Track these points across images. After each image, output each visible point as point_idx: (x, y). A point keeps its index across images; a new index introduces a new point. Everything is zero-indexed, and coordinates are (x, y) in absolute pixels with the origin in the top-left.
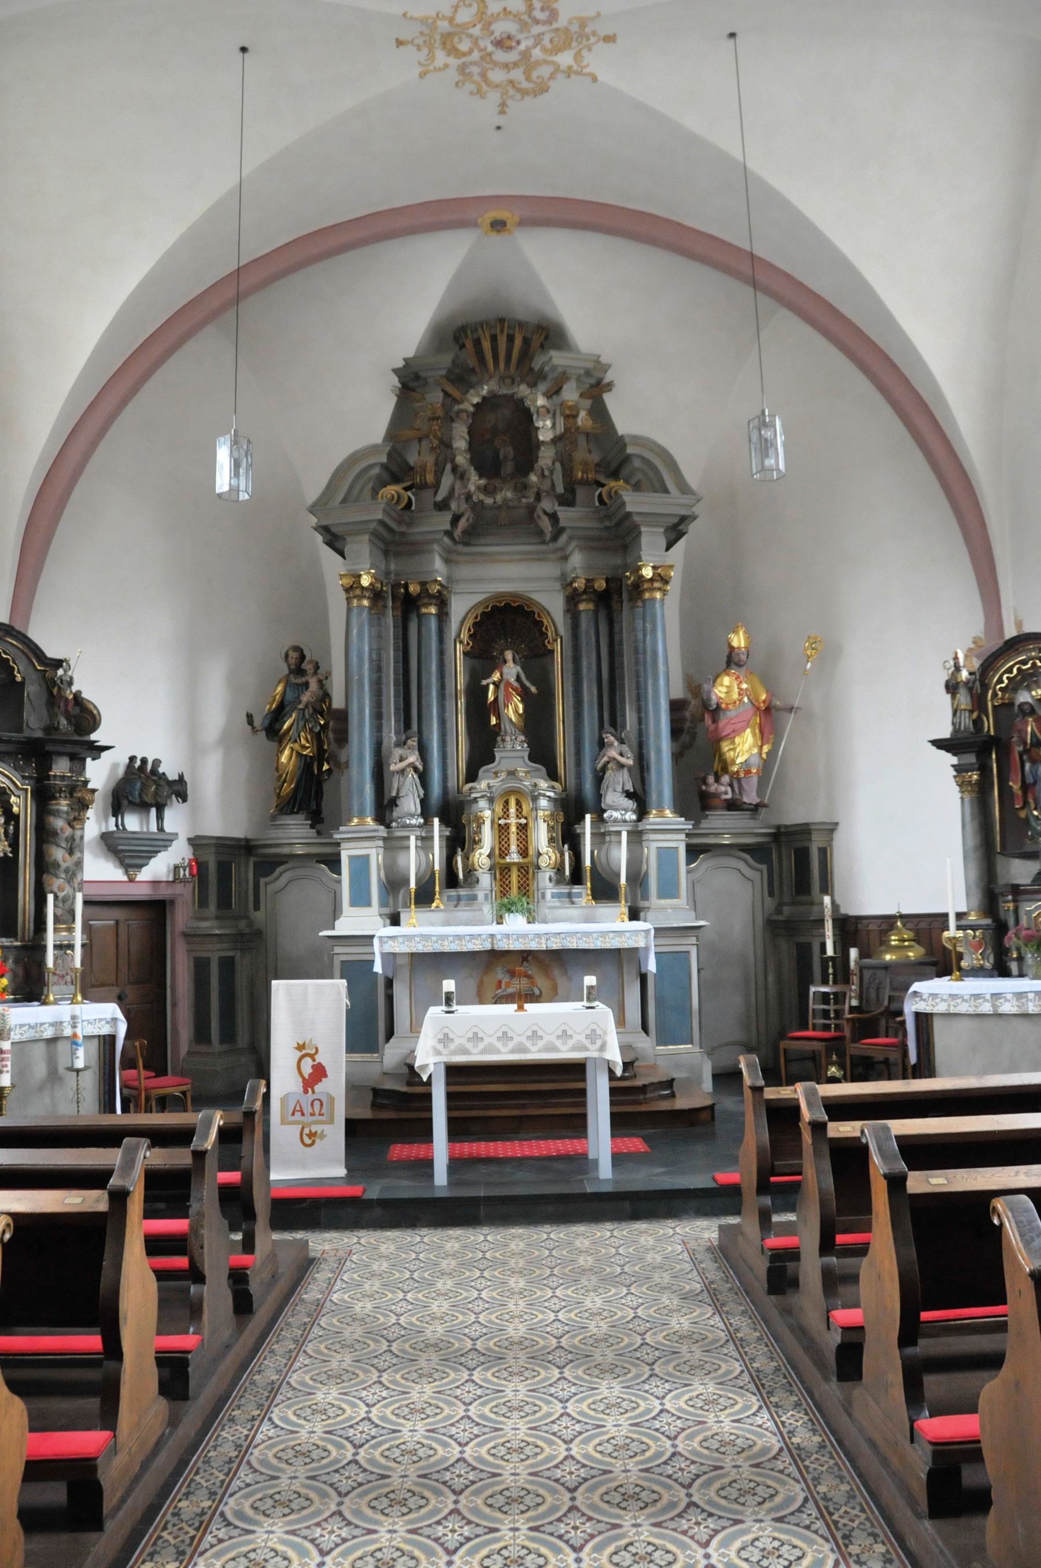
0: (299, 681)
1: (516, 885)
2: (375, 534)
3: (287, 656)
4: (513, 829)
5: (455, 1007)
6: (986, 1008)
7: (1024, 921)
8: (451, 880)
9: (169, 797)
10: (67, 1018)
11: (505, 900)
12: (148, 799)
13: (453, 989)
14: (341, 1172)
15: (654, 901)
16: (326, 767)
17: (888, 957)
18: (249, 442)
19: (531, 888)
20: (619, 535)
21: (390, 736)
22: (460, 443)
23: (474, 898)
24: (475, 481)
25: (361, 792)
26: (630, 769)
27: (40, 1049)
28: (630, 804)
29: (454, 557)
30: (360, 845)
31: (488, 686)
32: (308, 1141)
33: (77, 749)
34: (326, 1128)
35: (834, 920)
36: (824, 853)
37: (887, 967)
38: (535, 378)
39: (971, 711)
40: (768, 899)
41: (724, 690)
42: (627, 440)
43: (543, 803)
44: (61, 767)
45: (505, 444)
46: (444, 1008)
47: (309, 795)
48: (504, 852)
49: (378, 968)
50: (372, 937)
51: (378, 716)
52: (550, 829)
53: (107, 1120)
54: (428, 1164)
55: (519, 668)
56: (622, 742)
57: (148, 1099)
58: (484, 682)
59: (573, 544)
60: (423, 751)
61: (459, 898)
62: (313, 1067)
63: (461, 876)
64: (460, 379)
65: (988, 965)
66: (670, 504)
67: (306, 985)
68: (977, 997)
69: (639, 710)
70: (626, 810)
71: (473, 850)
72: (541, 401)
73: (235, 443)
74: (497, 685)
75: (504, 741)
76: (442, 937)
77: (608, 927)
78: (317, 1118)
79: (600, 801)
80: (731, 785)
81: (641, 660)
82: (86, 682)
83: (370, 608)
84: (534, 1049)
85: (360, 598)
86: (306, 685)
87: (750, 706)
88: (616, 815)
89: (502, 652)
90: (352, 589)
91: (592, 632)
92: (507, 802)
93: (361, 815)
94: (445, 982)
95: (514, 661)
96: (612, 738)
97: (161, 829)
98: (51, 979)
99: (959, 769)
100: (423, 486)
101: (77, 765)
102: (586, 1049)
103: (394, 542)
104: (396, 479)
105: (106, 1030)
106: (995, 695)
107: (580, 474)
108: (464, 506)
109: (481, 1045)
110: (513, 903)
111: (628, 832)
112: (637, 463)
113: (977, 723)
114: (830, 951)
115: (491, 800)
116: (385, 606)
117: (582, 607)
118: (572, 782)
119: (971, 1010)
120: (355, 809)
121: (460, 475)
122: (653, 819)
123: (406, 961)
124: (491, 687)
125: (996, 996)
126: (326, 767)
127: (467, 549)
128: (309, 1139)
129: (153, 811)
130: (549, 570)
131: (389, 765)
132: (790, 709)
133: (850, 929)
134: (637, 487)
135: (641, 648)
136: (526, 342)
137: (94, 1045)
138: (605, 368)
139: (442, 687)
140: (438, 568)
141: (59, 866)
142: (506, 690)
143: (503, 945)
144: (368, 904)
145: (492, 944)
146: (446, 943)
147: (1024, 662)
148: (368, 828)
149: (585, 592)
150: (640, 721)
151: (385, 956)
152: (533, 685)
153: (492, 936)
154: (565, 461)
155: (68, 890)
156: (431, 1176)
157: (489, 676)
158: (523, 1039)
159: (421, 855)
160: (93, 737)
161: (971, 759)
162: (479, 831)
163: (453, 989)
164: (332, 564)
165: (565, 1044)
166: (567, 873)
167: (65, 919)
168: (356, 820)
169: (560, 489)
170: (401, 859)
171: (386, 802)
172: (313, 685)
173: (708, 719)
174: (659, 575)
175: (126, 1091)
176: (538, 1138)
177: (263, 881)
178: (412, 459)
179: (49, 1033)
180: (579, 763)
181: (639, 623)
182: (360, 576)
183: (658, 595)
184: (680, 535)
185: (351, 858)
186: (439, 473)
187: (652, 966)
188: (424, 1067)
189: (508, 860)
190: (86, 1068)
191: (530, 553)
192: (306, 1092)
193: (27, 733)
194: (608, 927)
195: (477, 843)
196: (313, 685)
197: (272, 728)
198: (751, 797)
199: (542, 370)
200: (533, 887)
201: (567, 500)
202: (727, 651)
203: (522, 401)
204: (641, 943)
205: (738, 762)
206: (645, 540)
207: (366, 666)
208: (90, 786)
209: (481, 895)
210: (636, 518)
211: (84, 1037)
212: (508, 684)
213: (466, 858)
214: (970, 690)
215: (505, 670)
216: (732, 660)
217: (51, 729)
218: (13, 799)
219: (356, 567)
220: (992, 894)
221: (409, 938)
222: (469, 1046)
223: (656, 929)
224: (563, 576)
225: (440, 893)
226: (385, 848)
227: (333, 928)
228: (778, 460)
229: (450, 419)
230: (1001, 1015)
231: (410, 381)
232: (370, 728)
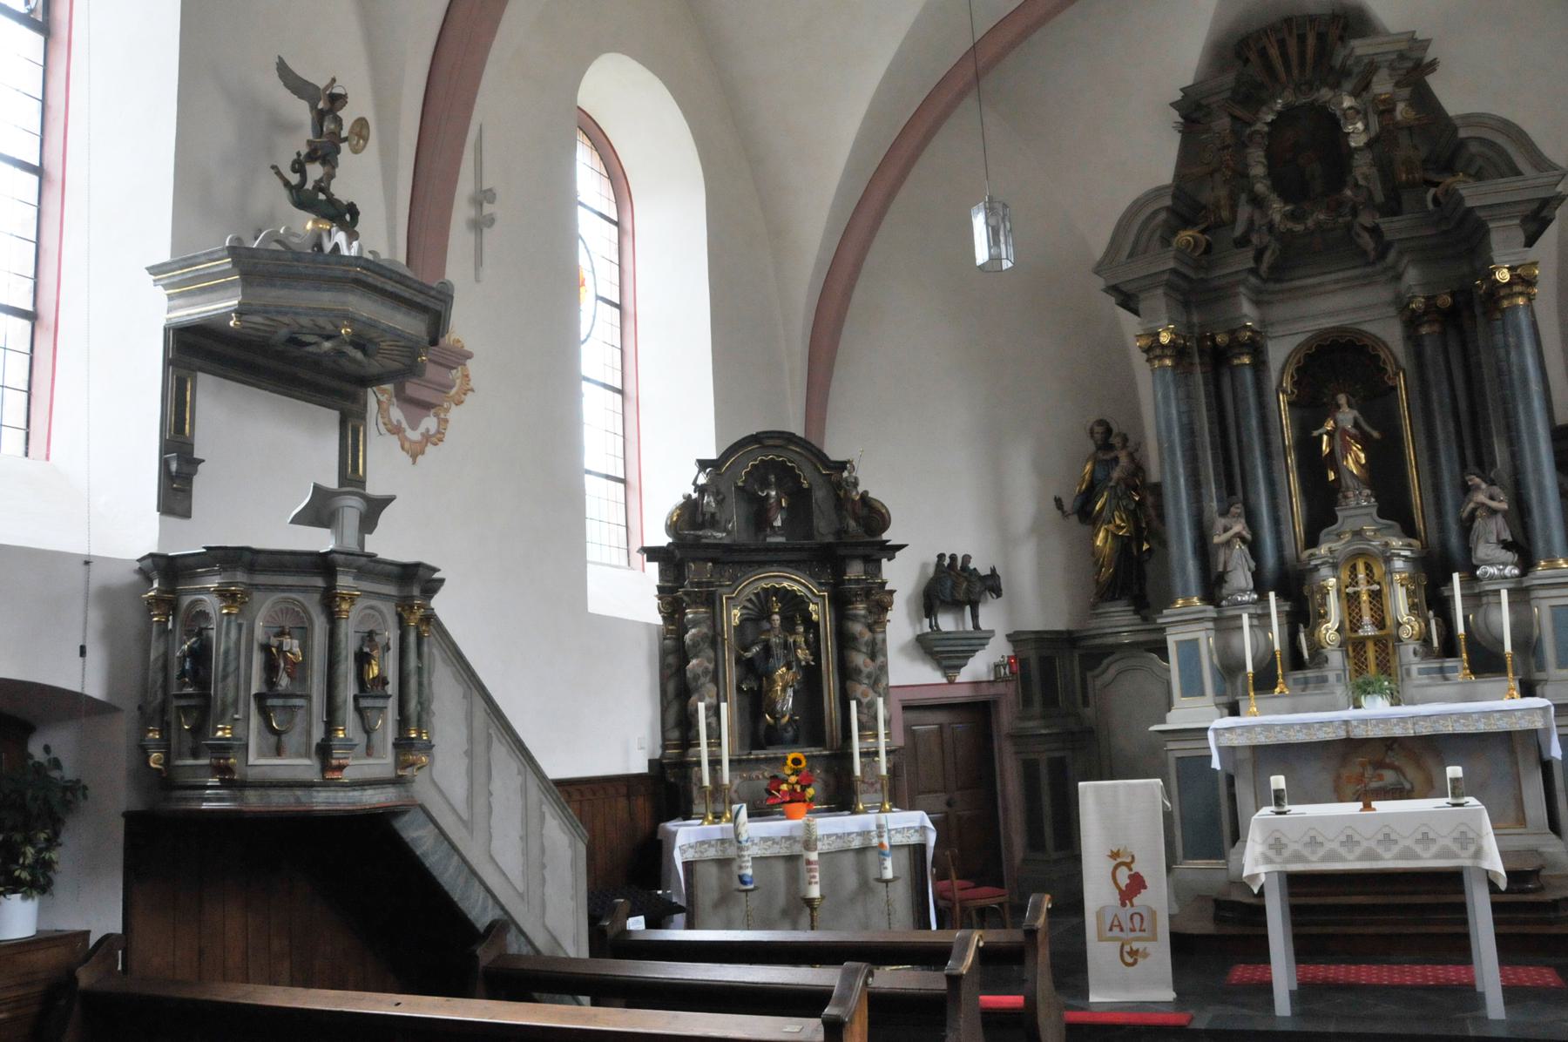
0: (1107, 457)
1: (1373, 662)
2: (1170, 286)
3: (1092, 432)
4: (1365, 597)
5: (1287, 807)
9: (981, 593)
10: (873, 828)
11: (1360, 680)
12: (961, 596)
14: (1169, 995)
15: (1553, 671)
16: (1146, 547)
18: (1005, 206)
19: (1392, 664)
20: (1464, 238)
21: (1213, 505)
22: (1258, 170)
23: (1324, 680)
24: (1277, 209)
25: (1184, 569)
26: (1505, 514)
27: (848, 861)
28: (1509, 556)
30: (1187, 628)
31: (1321, 437)
32: (1129, 960)
33: (868, 551)
34: (1150, 946)
38: (1336, 77)
42: (1458, 122)
43: (1398, 564)
44: (855, 570)
46: (1273, 808)
47: (1132, 578)
48: (1356, 625)
49: (1216, 764)
51: (1195, 484)
52: (1410, 594)
53: (920, 937)
54: (1267, 988)
55: (1356, 413)
56: (1492, 483)
57: (964, 910)
58: (1316, 433)
60: (1251, 518)
61: (1306, 682)
62: (1130, 877)
63: (1306, 655)
64: (1249, 96)
66: (1528, 186)
67: (1115, 786)
70: (1505, 564)
71: (1319, 625)
72: (1348, 102)
73: (990, 212)
74: (1330, 434)
75: (1346, 497)
76: (1287, 726)
77: (1500, 705)
78: (1138, 934)
79: (1470, 558)
82: (872, 482)
83: (1174, 367)
84: (1387, 855)
85: (1161, 357)
86: (1116, 460)
88: (1492, 570)
89: (1334, 397)
90: (1153, 349)
91: (1441, 359)
92: (1354, 568)
93: (1187, 597)
95: (1350, 406)
96: (1477, 480)
97: (976, 627)
98: (860, 787)
100: (1220, 224)
101: (871, 567)
102: (1456, 856)
103: (1193, 291)
104: (1187, 223)
105: (915, 839)
107: (1404, 177)
108: (1266, 239)
109: (1321, 852)
110: (1370, 684)
111: (1509, 591)
112: (1474, 148)
115: (1335, 566)
117: (1424, 330)
118: (1434, 537)
121: (1257, 202)
122: (1541, 570)
124: (1325, 438)
126: (1146, 547)
127: (1278, 286)
128: (1132, 957)
129: (968, 608)
130: (1381, 294)
134: (1479, 176)
136: (1321, 37)
137: (904, 855)
138: (1425, 44)
140: (1248, 313)
141: (860, 671)
142: (1343, 440)
143: (1360, 733)
144: (1202, 693)
149: (1425, 313)
151: (1222, 750)
152: (1375, 428)
153: (1346, 722)
154: (1385, 167)
155: (871, 695)
156: (1270, 1002)
157: (1322, 426)
158: (1373, 844)
159: (1258, 634)
160: (885, 536)
162: (1324, 604)
164: (1130, 325)
165: (1427, 849)
166: (1436, 644)
167: (868, 727)
169: (1379, 197)
170: (1235, 641)
171: (1213, 577)
172: (1124, 460)
174: (1519, 276)
175: (941, 903)
176: (1416, 962)
177: (1089, 675)
178: (1206, 197)
179: (856, 843)
182: (1158, 334)
183: (1521, 301)
184: (1544, 224)
185: (1179, 644)
186: (1233, 209)
187: (1556, 752)
188: (1254, 877)
189: (1361, 633)
190: (895, 878)
191: (1344, 280)
192: (1124, 904)
193: (818, 539)
194: (1500, 705)
195: (1324, 616)
196: (1124, 460)
197: (1084, 511)
199: (1343, 65)
200: (1394, 662)
201: (1392, 208)
204: (1539, 725)
206: (1496, 239)
207: (1176, 431)
208: (887, 587)
209: (1332, 676)
210: (1481, 214)
211: (892, 847)
212: (1345, 432)
213: (1310, 636)
215: (1340, 416)
217: (841, 532)
218: (812, 607)
221: (1249, 729)
222: (1306, 852)
225: (1284, 676)
226: (1217, 630)
227: (1163, 721)
229: (1242, 145)
231: (1193, 111)
232: (1188, 500)
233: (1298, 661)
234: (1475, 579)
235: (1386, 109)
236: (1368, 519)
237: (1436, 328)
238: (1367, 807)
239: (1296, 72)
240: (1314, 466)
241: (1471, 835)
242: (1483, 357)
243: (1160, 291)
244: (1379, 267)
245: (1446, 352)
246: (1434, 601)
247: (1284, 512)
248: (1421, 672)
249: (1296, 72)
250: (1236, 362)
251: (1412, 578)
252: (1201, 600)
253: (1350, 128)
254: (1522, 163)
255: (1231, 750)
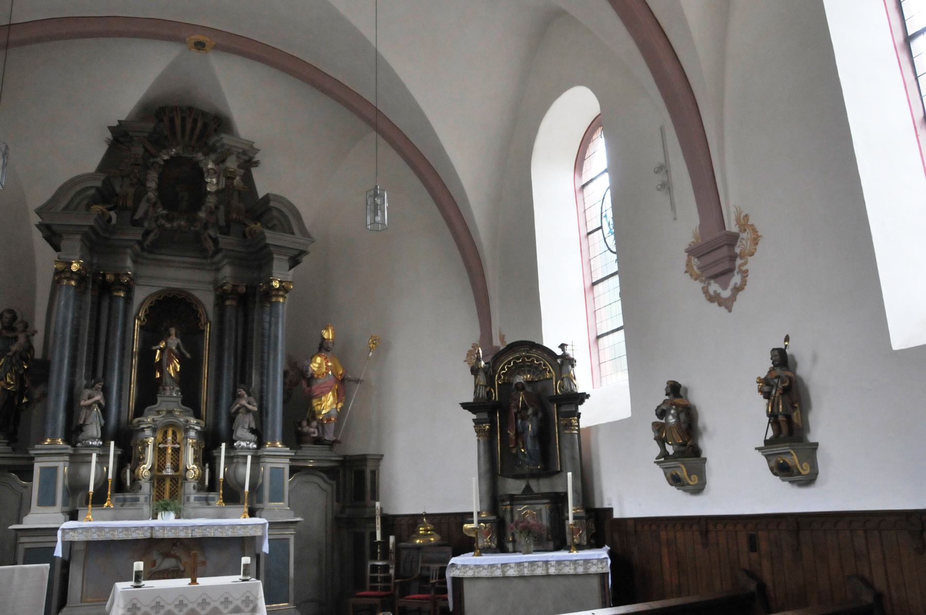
0: (10, 335)
1: (168, 492)
4: (170, 451)
6: (498, 573)
7: (516, 518)
8: (120, 487)
13: (142, 568)
15: (268, 505)
17: (418, 541)
20: (258, 259)
22: (152, 184)
23: (137, 500)
25: (55, 418)
29: (140, 260)
30: (51, 460)
35: (382, 518)
36: (374, 474)
37: (419, 548)
38: (209, 150)
39: (486, 387)
40: (335, 504)
41: (317, 365)
42: (271, 197)
43: (192, 434)
45: (182, 188)
48: (161, 467)
50: (58, 529)
51: (73, 365)
52: (195, 452)
55: (179, 341)
56: (249, 395)
58: (154, 348)
59: (225, 262)
60: (106, 391)
61: (125, 500)
64: (157, 141)
65: (493, 545)
67: (13, 570)
68: (492, 566)
69: (262, 374)
70: (251, 442)
72: (211, 166)
75: (164, 389)
77: (237, 521)
80: (317, 428)
81: (266, 342)
85: (69, 279)
86: (16, 339)
87: (332, 377)
88: (243, 444)
89: (167, 330)
93: (54, 437)
94: (136, 564)
95: (176, 336)
96: (243, 392)
99: (477, 422)
103: (98, 243)
106: (499, 377)
108: (154, 225)
110: (168, 504)
111: (252, 457)
112: (275, 213)
113: (489, 394)
114: (379, 538)
115: (154, 430)
116: (86, 288)
117: (228, 303)
118: (210, 420)
119: (489, 575)
120: (49, 431)
123: (83, 547)
124: (158, 352)
125: (504, 565)
127: (150, 256)
130: (207, 276)
131: (80, 401)
132: (358, 381)
133: (391, 523)
135: (267, 333)
136: (205, 125)
139: (123, 348)
142: (169, 355)
143: (159, 535)
144: (53, 504)
145: (151, 534)
146: (116, 533)
147: (518, 358)
148: (58, 446)
150: (262, 382)
153: (152, 528)
157: (158, 344)
161: (485, 416)
163: (142, 568)
165: (226, 608)
168: (49, 440)
169: (222, 222)
170: (83, 470)
171: (73, 428)
172: (22, 339)
173: (304, 384)
180: (217, 406)
181: (267, 318)
182: (71, 264)
183: (281, 300)
185: (43, 469)
191: (193, 263)
194: (237, 521)
198: (329, 437)
201: (225, 231)
202: (319, 341)
203: (197, 163)
204: (259, 533)
205: (324, 412)
209: (142, 498)
210: (272, 248)
212: (171, 351)
214: (486, 373)
215: (170, 341)
216: (323, 347)
219: (68, 257)
220: (495, 501)
223: (270, 523)
224: (215, 282)
226: (71, 462)
227: (21, 523)
228: (385, 216)
230: (579, 575)
231: (120, 136)
233: (121, 486)
234: (233, 448)
235: (230, 178)
236: (175, 404)
237: (234, 303)
238: (194, 582)
239: (187, 138)
240: (148, 366)
241: (251, 598)
242: (255, 326)
243: (79, 237)
244: (209, 261)
245: (237, 319)
246: (207, 458)
247: (125, 393)
248: (196, 499)
249: (187, 138)
250: (116, 294)
251: (197, 444)
252: (63, 441)
253: (208, 180)
254: (296, 230)
255: (72, 543)
